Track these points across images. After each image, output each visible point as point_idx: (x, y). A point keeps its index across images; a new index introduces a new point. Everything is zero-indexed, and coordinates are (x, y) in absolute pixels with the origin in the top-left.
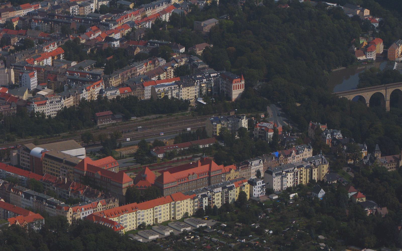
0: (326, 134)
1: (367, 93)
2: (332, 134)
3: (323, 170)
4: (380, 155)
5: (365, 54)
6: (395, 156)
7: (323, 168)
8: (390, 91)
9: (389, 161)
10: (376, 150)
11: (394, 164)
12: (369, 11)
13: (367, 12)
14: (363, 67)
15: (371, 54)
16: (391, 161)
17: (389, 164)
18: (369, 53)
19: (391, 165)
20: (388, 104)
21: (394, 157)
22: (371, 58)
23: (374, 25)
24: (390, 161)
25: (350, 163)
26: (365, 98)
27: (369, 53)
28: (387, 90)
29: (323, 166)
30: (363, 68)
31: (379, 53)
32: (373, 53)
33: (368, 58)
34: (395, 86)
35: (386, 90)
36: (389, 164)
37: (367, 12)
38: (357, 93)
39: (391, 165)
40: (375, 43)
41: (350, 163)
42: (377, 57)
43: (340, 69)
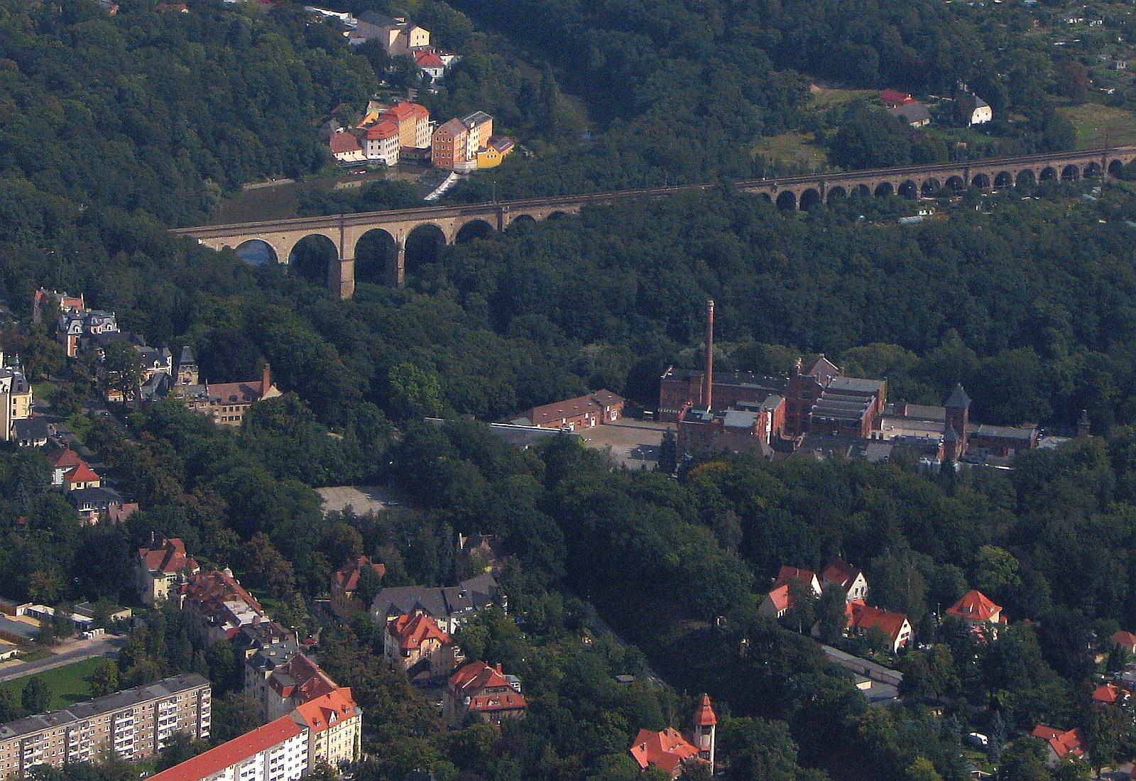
0: (69, 322)
1: (281, 235)
2: (86, 321)
3: (14, 411)
4: (195, 377)
5: (361, 146)
6: (247, 383)
7: (15, 403)
8: (355, 233)
10: (182, 361)
11: (241, 406)
12: (427, 34)
13: (420, 37)
14: (355, 183)
16: (234, 399)
18: (379, 142)
19: (231, 409)
20: (347, 271)
21: (243, 388)
22: (379, 157)
24: (230, 399)
25: (115, 399)
26: (275, 248)
27: (379, 142)
28: (346, 229)
29: (15, 400)
30: (355, 186)
32: (386, 143)
33: (369, 157)
35: (341, 228)
37: (420, 37)
39: (231, 409)
40: (396, 116)
41: (115, 399)
42: (401, 158)
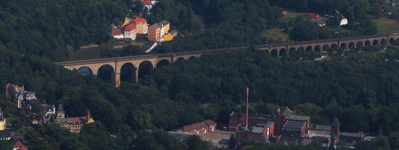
0: (19, 96)
1: (94, 65)
2: (25, 96)
4: (64, 115)
5: (123, 33)
8: (121, 64)
9: (75, 122)
15: (129, 33)
16: (77, 123)
17: (75, 126)
19: (76, 127)
20: (118, 77)
21: (81, 119)
22: (129, 37)
23: (148, 6)
25: (35, 123)
27: (129, 31)
28: (117, 63)
31: (141, 33)
33: (126, 37)
34: (127, 59)
35: (116, 62)
36: (75, 126)
38: (83, 64)
41: (35, 123)
43: (92, 47)
